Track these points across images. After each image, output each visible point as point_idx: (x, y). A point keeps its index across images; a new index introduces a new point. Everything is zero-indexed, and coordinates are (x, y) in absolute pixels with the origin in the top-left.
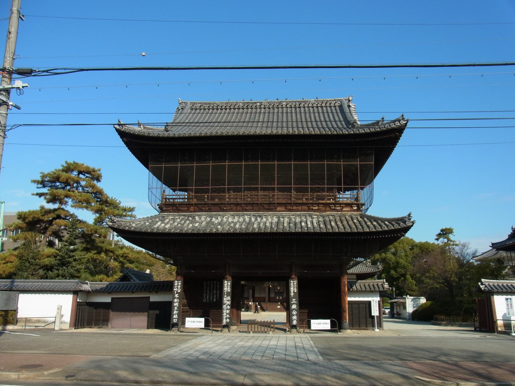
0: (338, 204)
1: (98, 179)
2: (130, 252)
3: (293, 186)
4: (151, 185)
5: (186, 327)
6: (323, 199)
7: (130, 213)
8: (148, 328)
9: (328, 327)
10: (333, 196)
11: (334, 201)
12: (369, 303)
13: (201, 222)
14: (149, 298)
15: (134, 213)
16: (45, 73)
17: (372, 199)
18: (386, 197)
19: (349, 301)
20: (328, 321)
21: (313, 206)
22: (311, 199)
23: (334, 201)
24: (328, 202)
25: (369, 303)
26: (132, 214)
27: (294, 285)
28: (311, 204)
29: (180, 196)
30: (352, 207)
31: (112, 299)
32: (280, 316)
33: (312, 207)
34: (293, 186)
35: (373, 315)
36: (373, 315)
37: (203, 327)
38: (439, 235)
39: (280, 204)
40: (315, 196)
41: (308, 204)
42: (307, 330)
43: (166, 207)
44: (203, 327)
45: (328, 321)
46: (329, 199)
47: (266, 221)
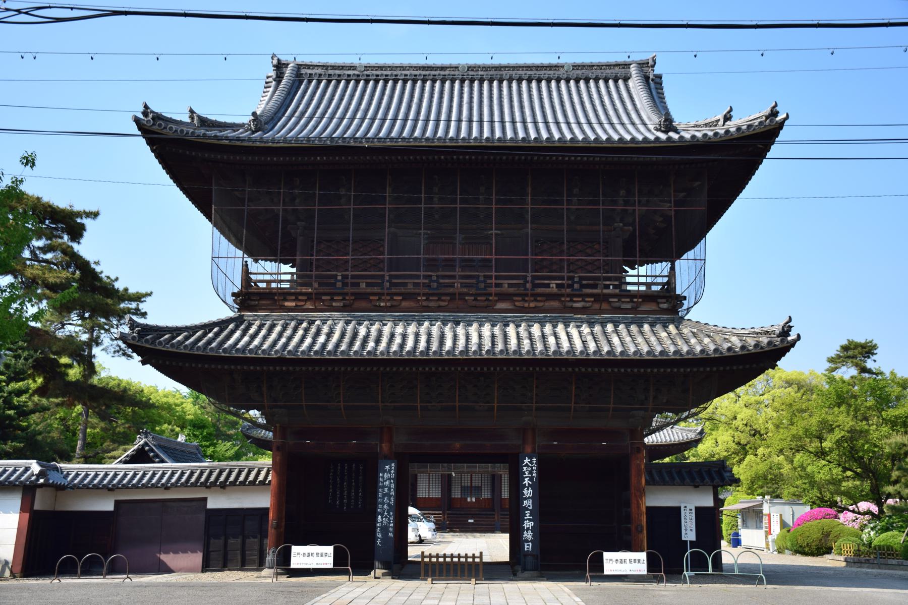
0: (627, 296)
1: (77, 232)
2: (785, 463)
3: (530, 257)
4: (216, 249)
5: (606, 573)
6: (595, 286)
7: (133, 305)
8: (203, 571)
9: (641, 568)
10: (616, 279)
11: (617, 291)
12: (677, 511)
13: (331, 334)
14: (205, 499)
15: (143, 307)
16: (23, 18)
17: (702, 287)
18: (731, 280)
19: (648, 508)
20: (330, 549)
21: (571, 301)
22: (569, 286)
23: (617, 291)
24: (605, 291)
25: (677, 511)
26: (137, 309)
27: (531, 473)
28: (568, 295)
29: (276, 273)
30: (658, 303)
31: (117, 503)
32: (495, 547)
33: (570, 304)
34: (530, 257)
35: (683, 539)
36: (683, 539)
37: (331, 566)
38: (836, 361)
39: (503, 297)
40: (576, 280)
41: (562, 295)
42: (594, 579)
43: (250, 298)
44: (331, 566)
45: (330, 549)
46: (607, 287)
47: (474, 337)
